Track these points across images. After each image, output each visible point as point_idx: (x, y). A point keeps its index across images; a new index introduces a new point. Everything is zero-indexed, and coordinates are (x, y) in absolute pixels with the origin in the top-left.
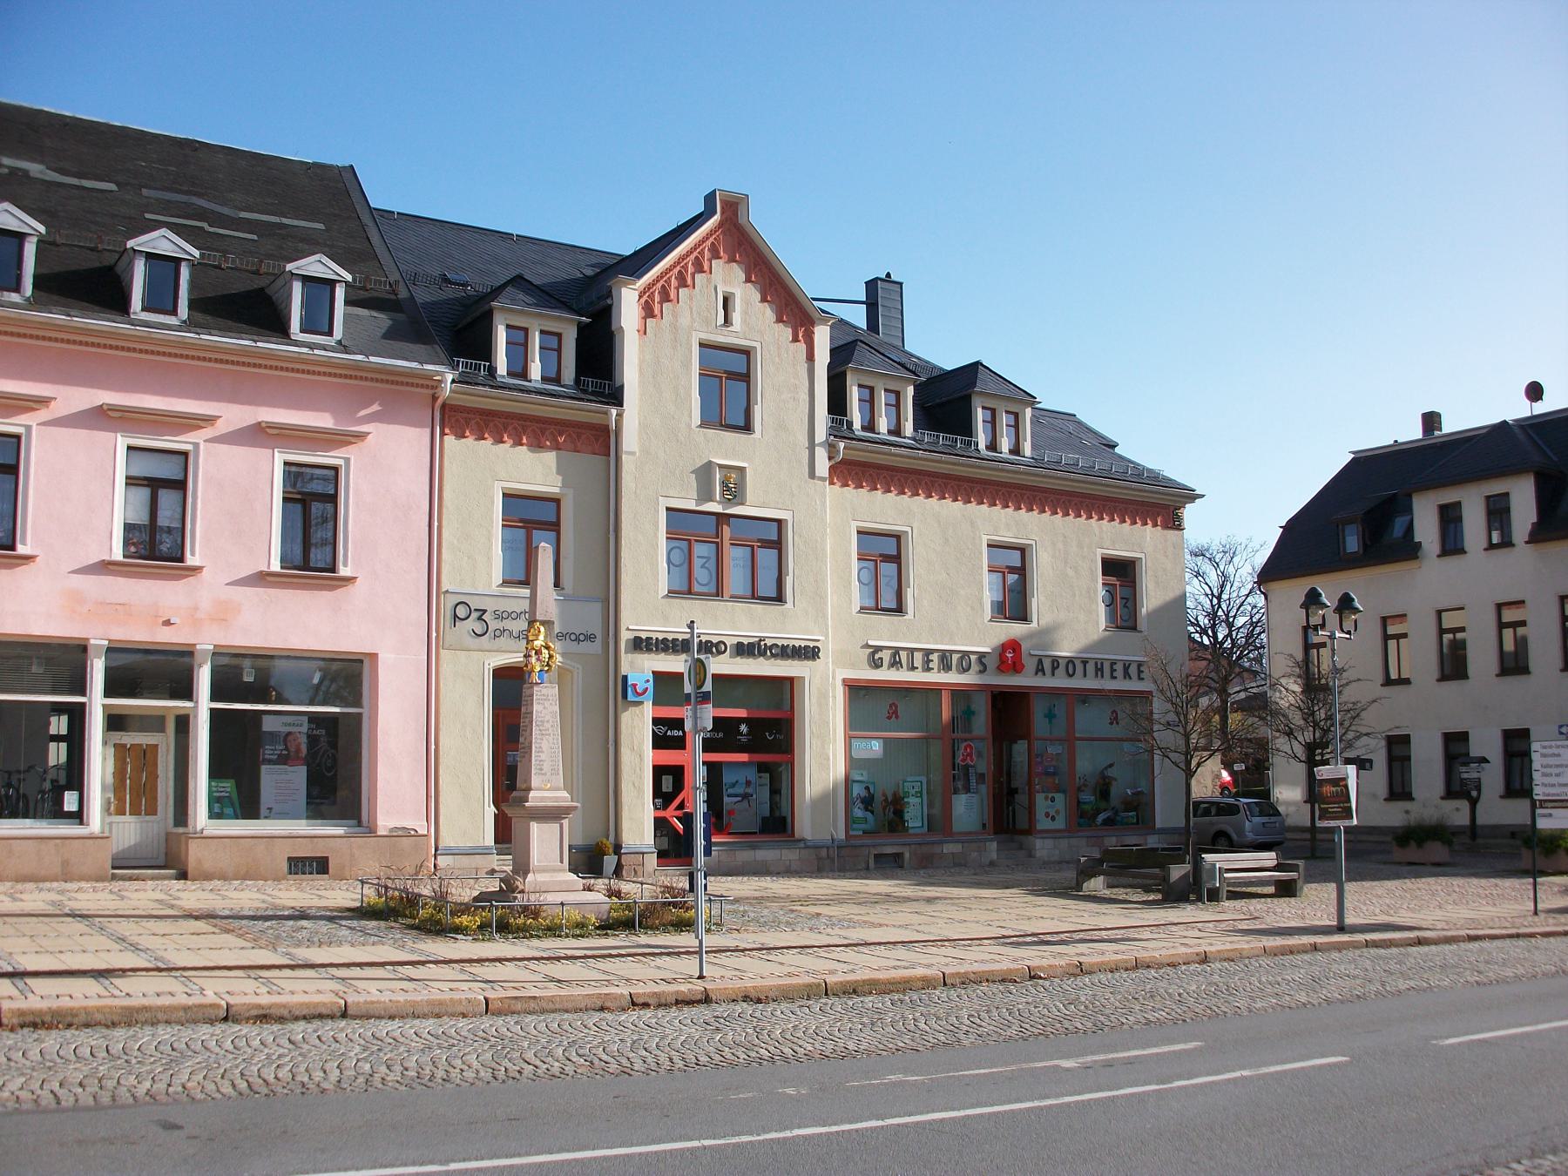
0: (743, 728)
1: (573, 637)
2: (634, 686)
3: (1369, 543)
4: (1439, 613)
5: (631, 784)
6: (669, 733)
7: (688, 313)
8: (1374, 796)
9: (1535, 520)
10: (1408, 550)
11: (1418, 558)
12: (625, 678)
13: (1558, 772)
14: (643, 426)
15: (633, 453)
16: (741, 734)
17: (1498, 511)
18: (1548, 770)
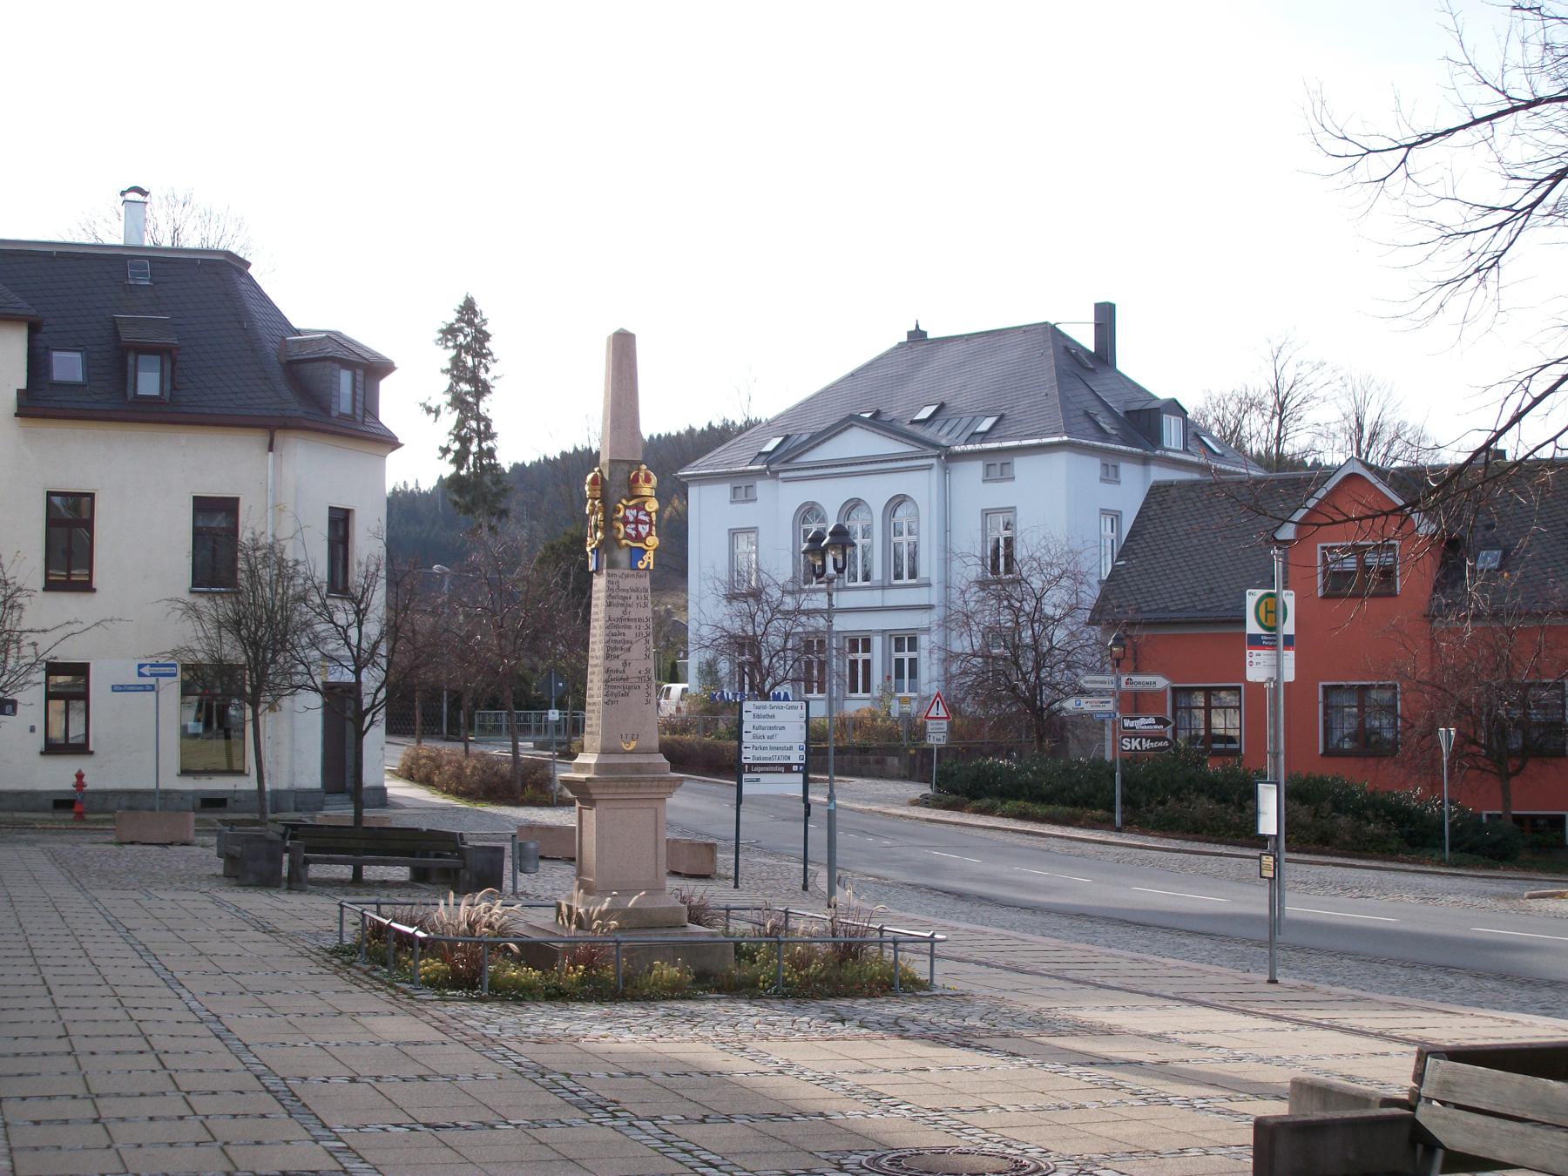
13: (771, 734)
18: (760, 732)
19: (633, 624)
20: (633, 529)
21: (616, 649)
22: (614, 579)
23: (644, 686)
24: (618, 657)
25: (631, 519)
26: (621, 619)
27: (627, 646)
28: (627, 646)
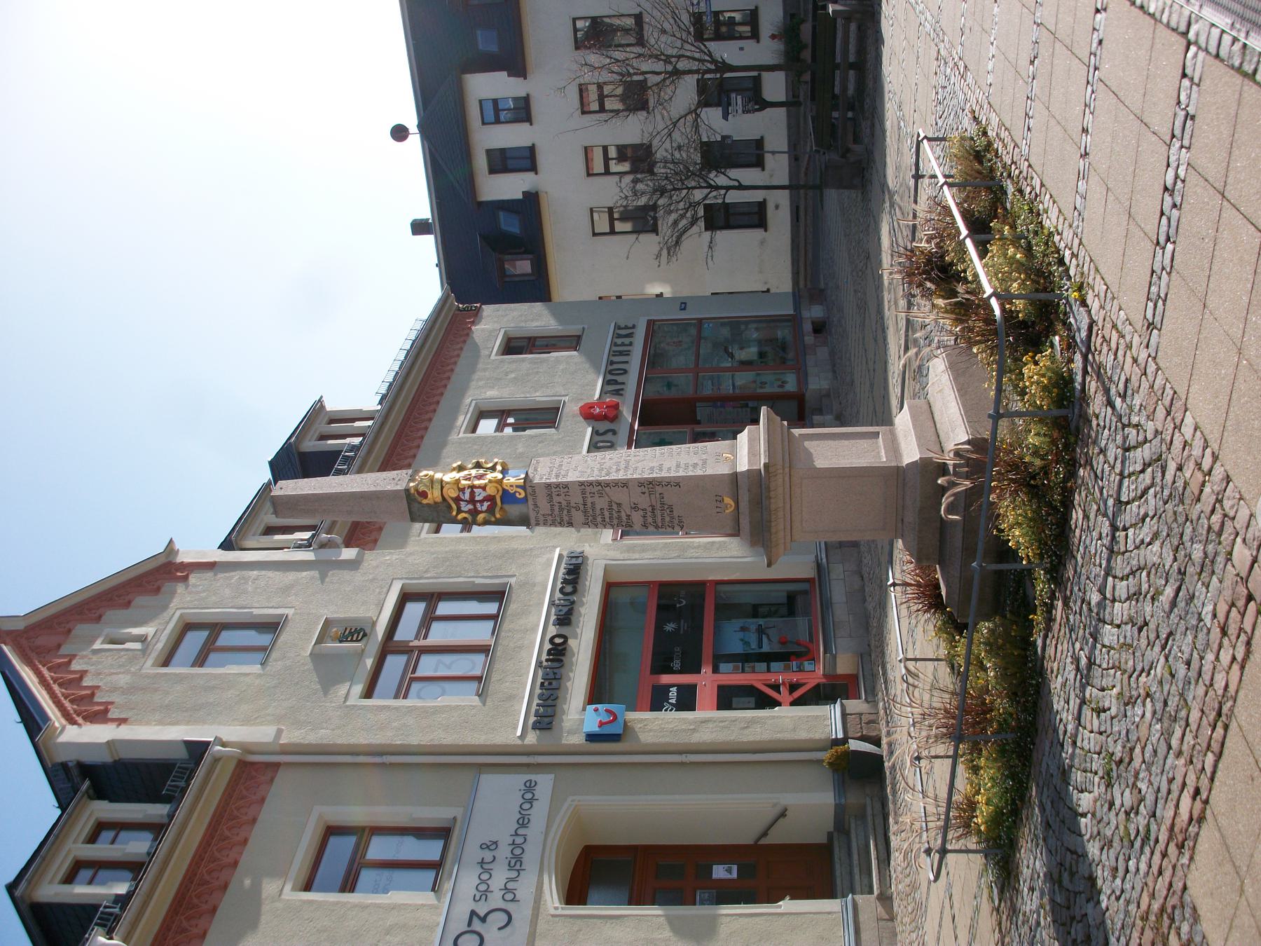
0: (670, 627)
1: (526, 806)
2: (601, 724)
3: (523, 249)
4: (595, 234)
5: (747, 732)
6: (673, 701)
7: (115, 678)
8: (762, 242)
9: (505, 73)
10: (530, 205)
11: (537, 193)
12: (591, 737)
14: (247, 721)
15: (279, 732)
16: (678, 630)
17: (496, 113)
19: (589, 500)
20: (482, 506)
21: (619, 518)
22: (541, 518)
23: (659, 489)
24: (629, 516)
25: (470, 507)
26: (585, 512)
27: (615, 507)
28: (615, 507)
